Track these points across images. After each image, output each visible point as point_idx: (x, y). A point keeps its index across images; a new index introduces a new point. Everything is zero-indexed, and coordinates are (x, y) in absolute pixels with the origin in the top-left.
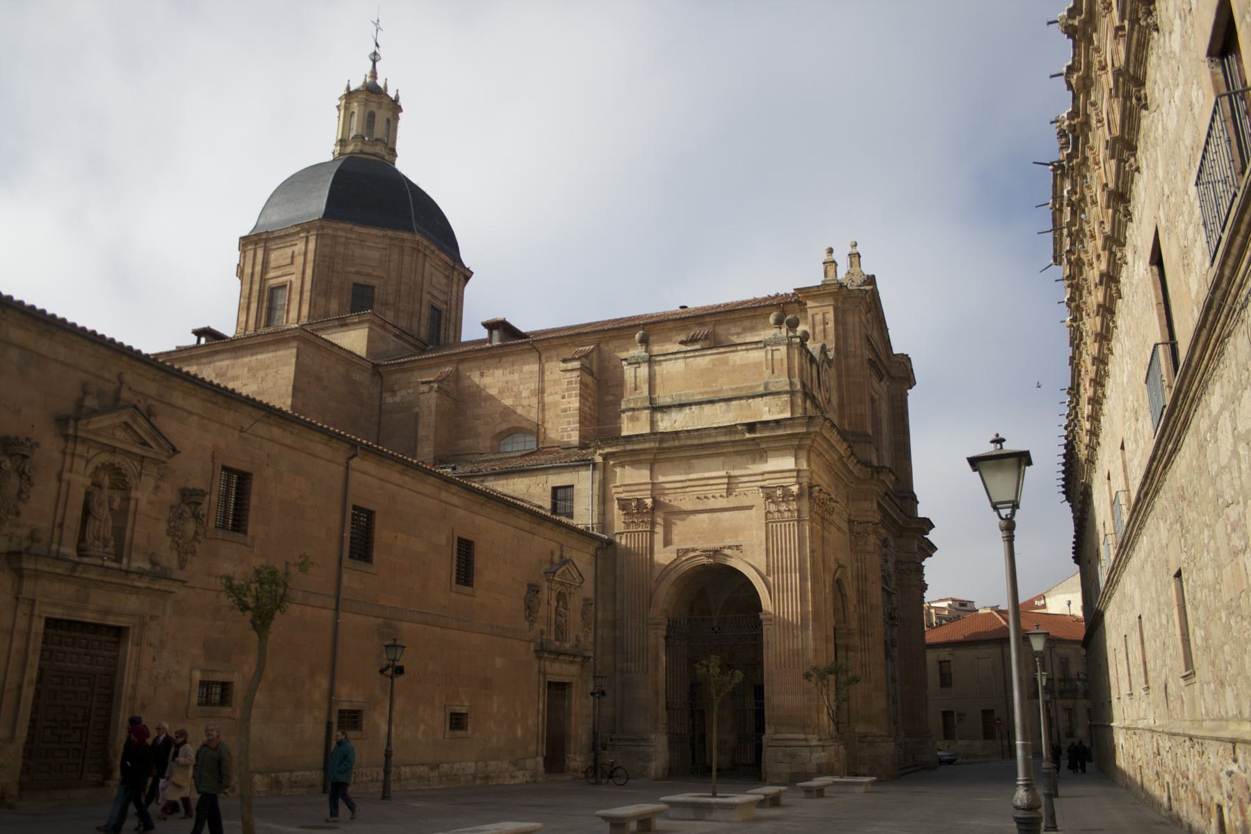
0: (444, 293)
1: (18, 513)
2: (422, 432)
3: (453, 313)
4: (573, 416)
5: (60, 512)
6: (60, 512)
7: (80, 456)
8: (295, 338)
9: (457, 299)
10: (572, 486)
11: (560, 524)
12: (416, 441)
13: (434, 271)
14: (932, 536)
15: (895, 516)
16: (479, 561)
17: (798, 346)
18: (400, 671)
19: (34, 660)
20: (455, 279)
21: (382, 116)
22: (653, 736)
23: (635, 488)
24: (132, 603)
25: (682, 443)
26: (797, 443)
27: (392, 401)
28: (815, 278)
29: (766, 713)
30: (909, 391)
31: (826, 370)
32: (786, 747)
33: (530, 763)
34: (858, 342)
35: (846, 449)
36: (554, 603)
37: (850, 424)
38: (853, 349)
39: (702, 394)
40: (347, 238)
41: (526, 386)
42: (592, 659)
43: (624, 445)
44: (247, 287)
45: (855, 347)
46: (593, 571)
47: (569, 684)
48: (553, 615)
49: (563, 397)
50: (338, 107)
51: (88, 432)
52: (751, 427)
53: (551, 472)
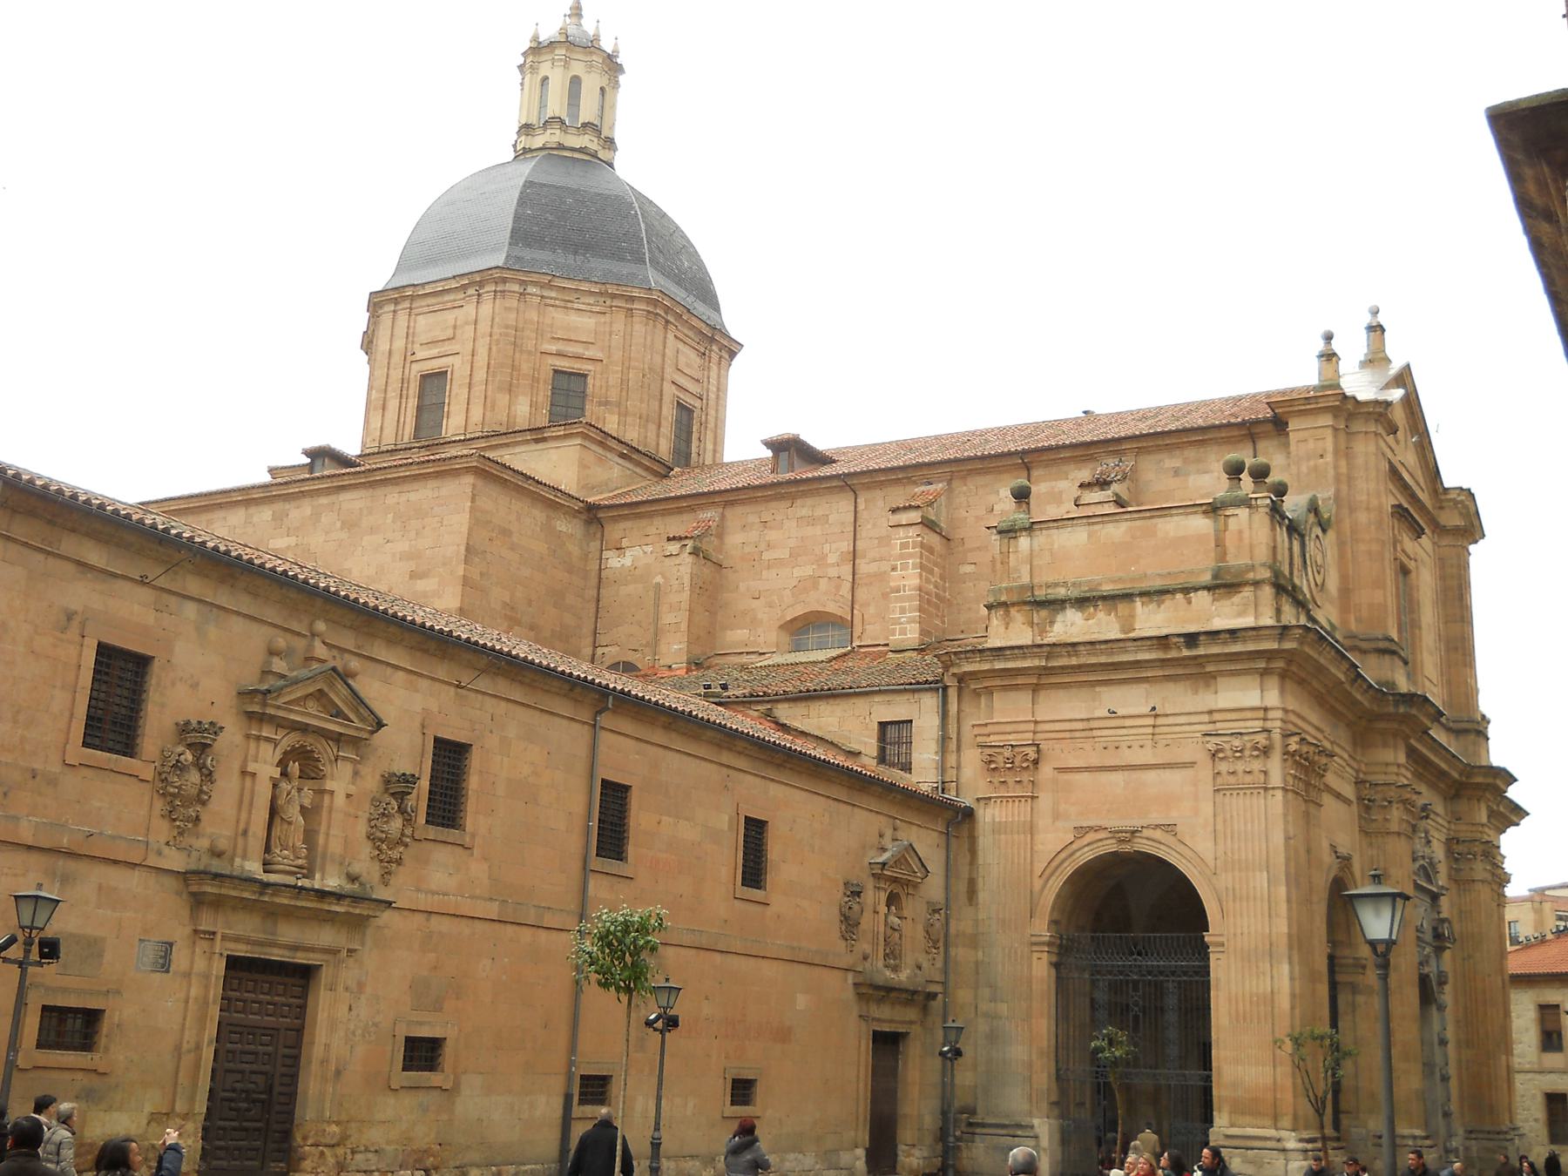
0: (698, 381)
1: (198, 819)
2: (668, 618)
3: (712, 412)
4: (910, 599)
5: (244, 815)
6: (244, 815)
7: (268, 739)
8: (468, 470)
9: (718, 389)
10: (911, 721)
11: (891, 788)
12: (657, 634)
13: (681, 346)
14: (1513, 793)
15: (1443, 766)
16: (775, 850)
17: (1267, 510)
18: (672, 1023)
19: (215, 1012)
20: (715, 357)
21: (592, 83)
22: (1036, 1122)
23: (1009, 728)
24: (326, 936)
25: (1083, 660)
26: (1263, 665)
27: (619, 565)
28: (1303, 375)
29: (1215, 1092)
30: (1472, 548)
31: (1317, 537)
32: (1247, 1149)
33: (845, 1158)
34: (1372, 485)
35: (1348, 670)
36: (883, 909)
37: (1359, 620)
38: (1364, 498)
39: (1114, 581)
40: (542, 297)
41: (834, 546)
42: (940, 996)
43: (991, 661)
44: (381, 373)
45: (1368, 495)
46: (943, 858)
47: (904, 1035)
48: (882, 929)
49: (894, 569)
50: (521, 67)
51: (279, 707)
52: (1191, 639)
53: (877, 699)
